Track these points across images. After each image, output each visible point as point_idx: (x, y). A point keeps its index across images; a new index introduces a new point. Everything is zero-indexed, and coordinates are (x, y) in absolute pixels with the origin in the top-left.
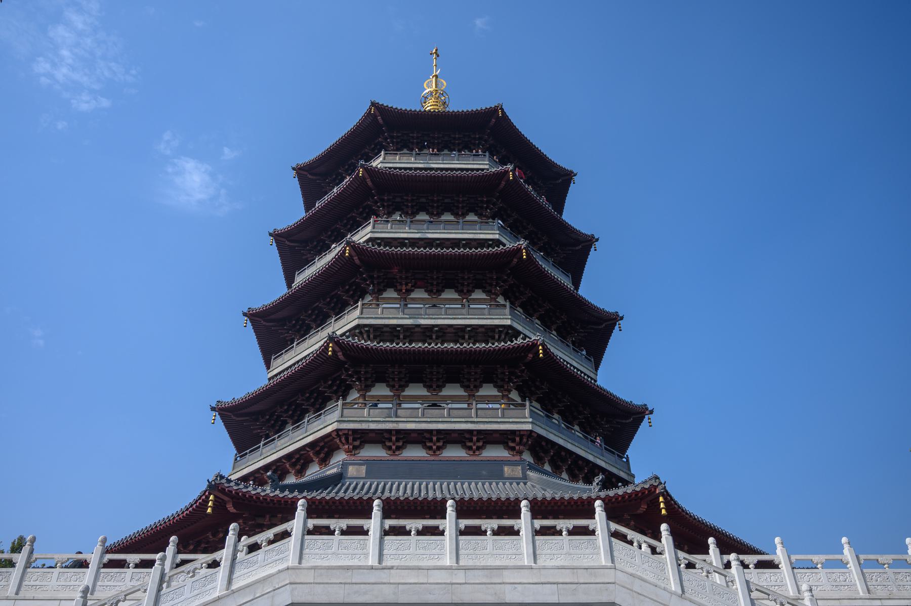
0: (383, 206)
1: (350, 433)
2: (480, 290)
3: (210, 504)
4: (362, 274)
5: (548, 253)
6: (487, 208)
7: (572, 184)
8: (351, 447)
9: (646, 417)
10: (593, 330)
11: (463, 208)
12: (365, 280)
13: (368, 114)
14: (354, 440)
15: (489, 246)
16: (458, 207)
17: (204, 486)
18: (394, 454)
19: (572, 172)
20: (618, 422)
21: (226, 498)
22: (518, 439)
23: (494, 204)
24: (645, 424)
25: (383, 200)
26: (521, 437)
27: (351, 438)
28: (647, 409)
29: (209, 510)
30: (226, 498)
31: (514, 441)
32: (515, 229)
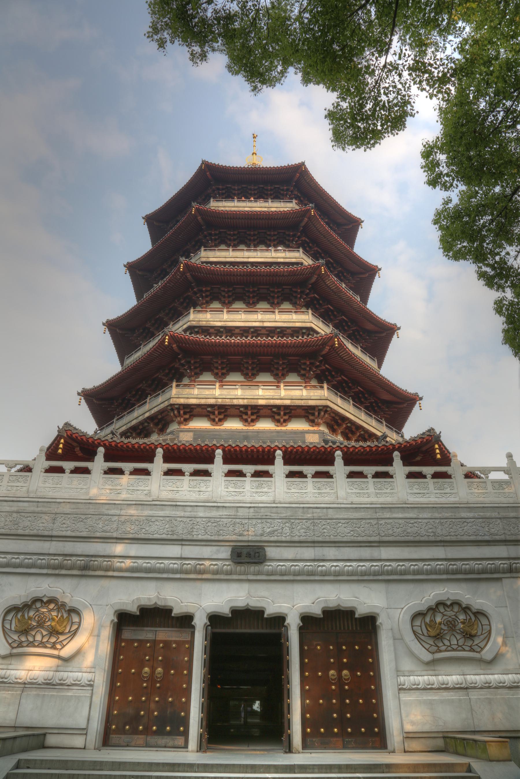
0: (212, 240)
1: (181, 407)
2: (288, 303)
3: (61, 446)
4: (179, 360)
5: (354, 338)
6: (301, 297)
7: (360, 229)
8: (182, 419)
9: (418, 402)
10: (378, 336)
11: (278, 297)
12: (183, 365)
13: (201, 167)
14: (185, 413)
15: (303, 334)
16: (273, 297)
17: (56, 434)
18: (217, 424)
19: (395, 325)
20: (395, 405)
21: (75, 444)
22: (317, 414)
23: (307, 295)
24: (416, 408)
25: (201, 291)
26: (320, 410)
27: (182, 412)
28: (418, 396)
29: (60, 451)
30: (75, 444)
31: (313, 414)
32: (325, 316)
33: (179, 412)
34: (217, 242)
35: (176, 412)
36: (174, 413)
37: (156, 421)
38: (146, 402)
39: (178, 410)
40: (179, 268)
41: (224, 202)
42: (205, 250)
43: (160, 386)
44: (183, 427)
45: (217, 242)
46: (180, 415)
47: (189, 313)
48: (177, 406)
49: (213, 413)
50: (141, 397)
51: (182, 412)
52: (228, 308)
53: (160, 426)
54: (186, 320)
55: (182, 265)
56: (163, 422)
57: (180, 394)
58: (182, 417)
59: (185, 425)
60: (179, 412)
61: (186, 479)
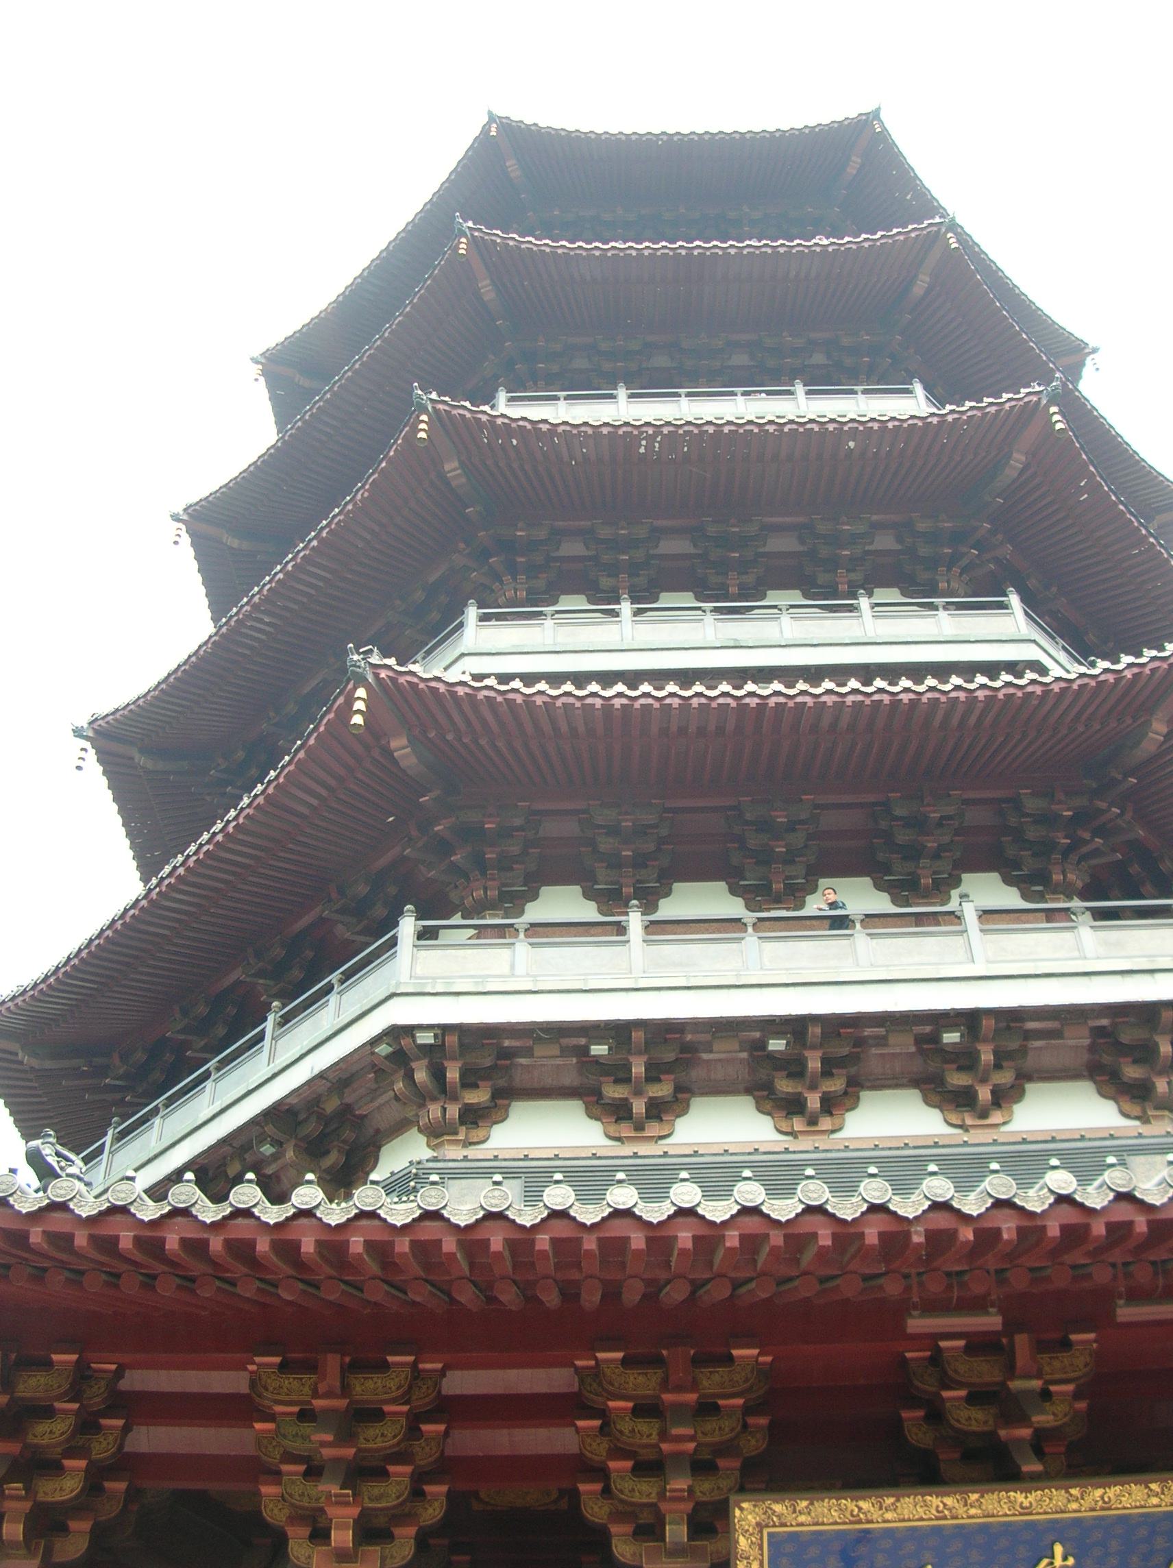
8: (453, 1111)
14: (470, 1080)
27: (453, 1074)
33: (438, 1074)
34: (541, 583)
35: (421, 1076)
36: (409, 1076)
37: (311, 1128)
38: (260, 1038)
40: (347, 710)
41: (562, 404)
42: (484, 618)
43: (314, 948)
44: (453, 1152)
45: (541, 583)
46: (442, 1088)
47: (393, 942)
48: (426, 1038)
49: (621, 1074)
50: (229, 1027)
51: (453, 1074)
52: (649, 906)
53: (333, 1158)
54: (371, 986)
55: (361, 692)
56: (348, 1134)
57: (437, 980)
58: (455, 1098)
59: (468, 1143)
60: (438, 1074)
61: (562, 403)
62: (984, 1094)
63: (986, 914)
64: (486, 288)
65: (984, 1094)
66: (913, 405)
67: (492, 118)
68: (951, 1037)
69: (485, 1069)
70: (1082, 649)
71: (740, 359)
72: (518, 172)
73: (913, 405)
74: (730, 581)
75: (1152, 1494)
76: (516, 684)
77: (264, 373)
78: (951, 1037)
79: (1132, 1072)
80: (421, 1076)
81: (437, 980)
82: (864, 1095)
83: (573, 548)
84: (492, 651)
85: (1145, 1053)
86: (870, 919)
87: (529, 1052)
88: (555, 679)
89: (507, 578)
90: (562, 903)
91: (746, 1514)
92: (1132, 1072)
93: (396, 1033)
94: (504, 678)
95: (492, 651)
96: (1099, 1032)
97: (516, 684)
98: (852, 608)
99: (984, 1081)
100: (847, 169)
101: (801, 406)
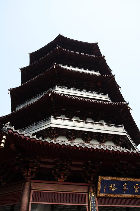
8: (54, 136)
27: (55, 132)
33: (53, 132)
35: (52, 132)
39: (54, 130)
43: (46, 118)
48: (53, 128)
51: (55, 132)
57: (56, 122)
58: (55, 134)
60: (53, 132)
62: (72, 138)
63: (75, 121)
64: (59, 53)
65: (72, 138)
66: (98, 74)
67: (60, 35)
68: (86, 134)
69: (59, 132)
70: (113, 101)
71: (81, 65)
72: (61, 40)
73: (98, 74)
74: (79, 87)
75: (133, 180)
76: (65, 95)
77: (30, 56)
78: (86, 134)
79: (117, 141)
80: (52, 132)
81: (56, 122)
82: (59, 136)
83: (65, 81)
84: (60, 90)
85: (118, 140)
86: (64, 119)
87: (80, 133)
88: (69, 95)
89: (58, 83)
90: (63, 117)
91: (100, 178)
92: (117, 141)
93: (51, 127)
94: (64, 94)
95: (60, 90)
96: (83, 133)
97: (65, 95)
98: (70, 89)
99: (103, 140)
100: (94, 48)
101: (88, 71)
